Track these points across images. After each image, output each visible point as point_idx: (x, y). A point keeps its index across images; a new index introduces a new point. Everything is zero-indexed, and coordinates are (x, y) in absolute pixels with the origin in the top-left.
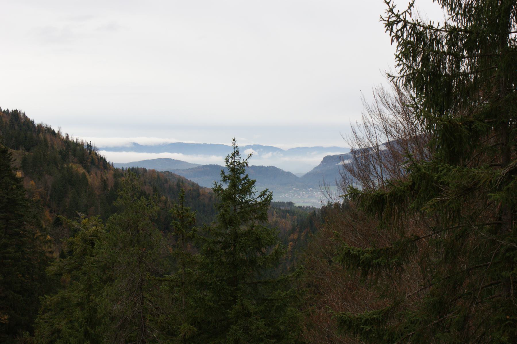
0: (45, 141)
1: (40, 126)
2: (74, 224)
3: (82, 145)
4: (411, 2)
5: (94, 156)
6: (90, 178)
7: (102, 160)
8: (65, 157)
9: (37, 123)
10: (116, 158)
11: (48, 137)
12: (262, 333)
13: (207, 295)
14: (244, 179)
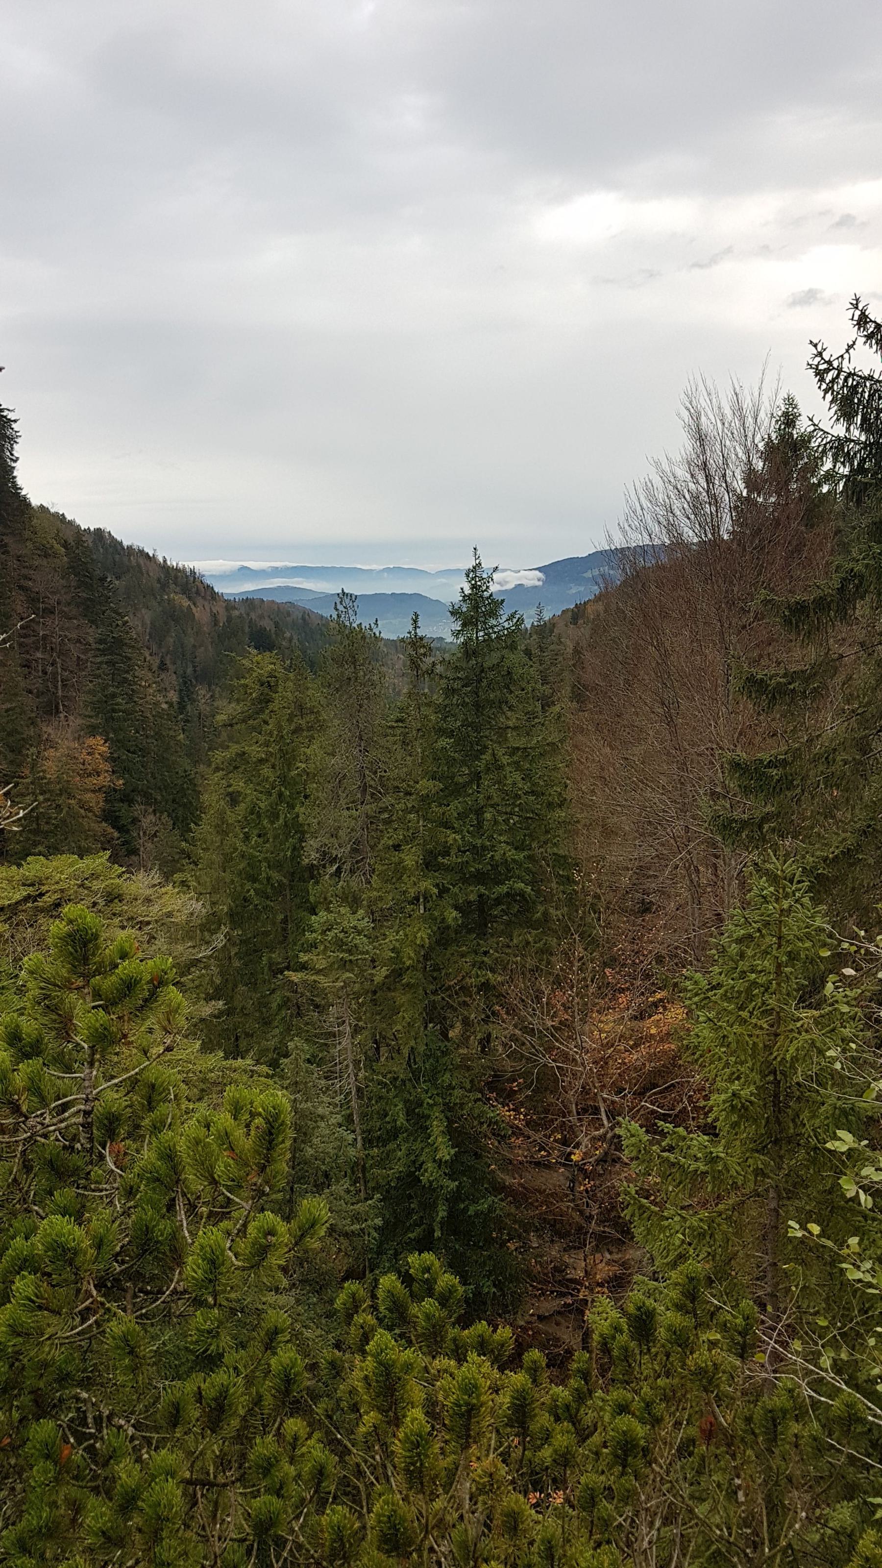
0: (139, 565)
1: (130, 548)
2: (244, 662)
3: (183, 571)
4: (851, 343)
5: (199, 584)
6: (197, 612)
7: (209, 588)
8: (164, 586)
9: (126, 543)
10: (227, 589)
11: (141, 561)
12: (520, 789)
13: (444, 742)
14: (487, 598)
